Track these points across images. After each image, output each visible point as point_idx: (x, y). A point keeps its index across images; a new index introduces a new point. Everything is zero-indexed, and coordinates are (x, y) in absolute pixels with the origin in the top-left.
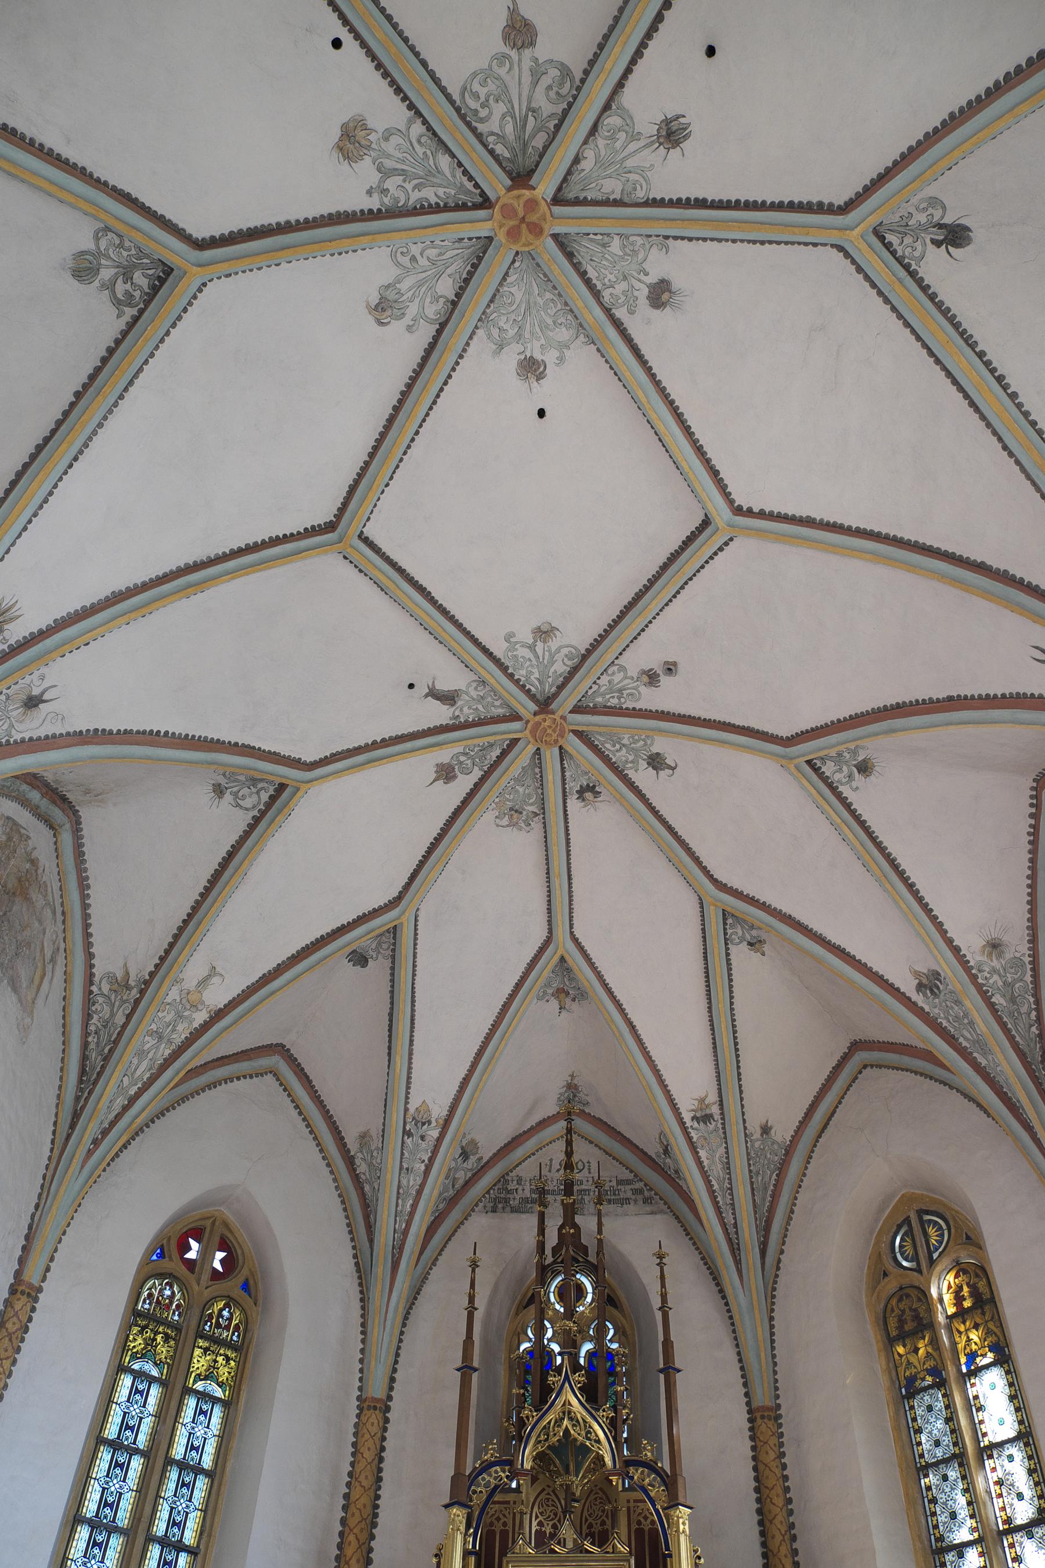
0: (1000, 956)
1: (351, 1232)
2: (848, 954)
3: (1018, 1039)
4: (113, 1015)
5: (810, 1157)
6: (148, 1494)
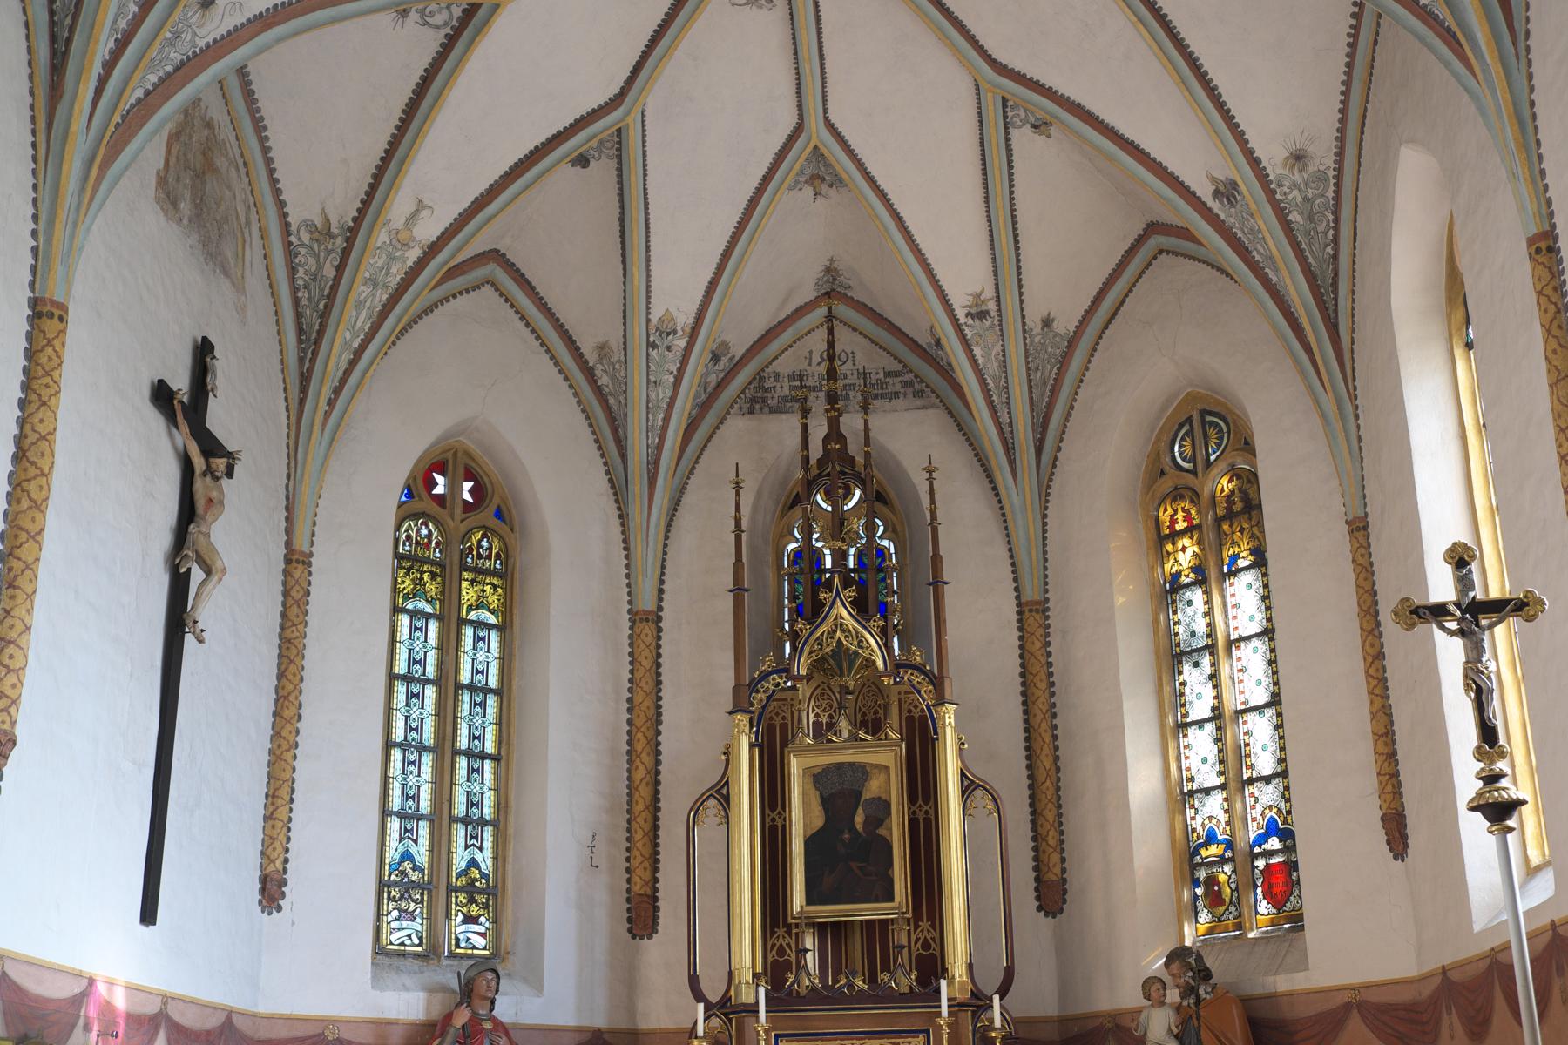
0: (1303, 169)
1: (600, 448)
2: (1142, 151)
3: (1311, 260)
4: (320, 267)
5: (1095, 350)
6: (446, 716)
